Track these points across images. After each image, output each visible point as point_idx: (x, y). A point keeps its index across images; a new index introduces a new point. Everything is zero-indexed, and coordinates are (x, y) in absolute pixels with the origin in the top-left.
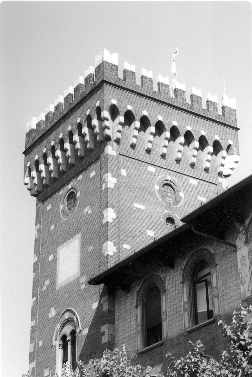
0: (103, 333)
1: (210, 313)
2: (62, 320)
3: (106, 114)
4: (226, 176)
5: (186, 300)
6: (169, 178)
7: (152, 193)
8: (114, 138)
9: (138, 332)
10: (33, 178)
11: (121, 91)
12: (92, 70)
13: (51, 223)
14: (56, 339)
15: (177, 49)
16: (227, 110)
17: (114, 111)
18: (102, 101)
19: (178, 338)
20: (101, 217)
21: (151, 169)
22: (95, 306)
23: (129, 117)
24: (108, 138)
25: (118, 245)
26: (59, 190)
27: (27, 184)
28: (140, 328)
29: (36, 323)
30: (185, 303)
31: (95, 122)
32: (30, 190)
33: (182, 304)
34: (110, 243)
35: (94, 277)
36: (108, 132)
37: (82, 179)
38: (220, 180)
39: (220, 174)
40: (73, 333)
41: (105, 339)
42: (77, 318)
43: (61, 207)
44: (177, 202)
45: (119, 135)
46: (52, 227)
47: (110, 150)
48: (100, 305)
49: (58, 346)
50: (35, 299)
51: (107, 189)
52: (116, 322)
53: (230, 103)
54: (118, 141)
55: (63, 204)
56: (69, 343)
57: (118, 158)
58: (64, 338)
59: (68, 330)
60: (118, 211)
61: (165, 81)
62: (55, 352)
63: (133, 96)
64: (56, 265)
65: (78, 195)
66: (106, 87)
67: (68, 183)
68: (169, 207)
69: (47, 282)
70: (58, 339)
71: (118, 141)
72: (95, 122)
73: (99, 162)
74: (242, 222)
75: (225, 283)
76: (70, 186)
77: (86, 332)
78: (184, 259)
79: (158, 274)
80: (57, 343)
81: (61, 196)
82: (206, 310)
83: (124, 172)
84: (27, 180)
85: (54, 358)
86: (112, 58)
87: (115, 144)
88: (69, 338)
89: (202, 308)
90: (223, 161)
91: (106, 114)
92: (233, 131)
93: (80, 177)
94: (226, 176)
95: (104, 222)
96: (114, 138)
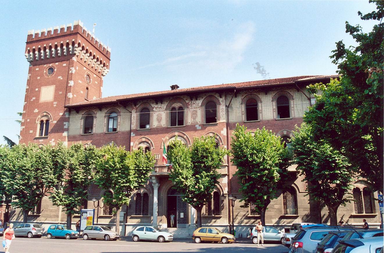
0: (65, 125)
1: (114, 130)
2: (42, 115)
3: (76, 45)
4: (104, 76)
5: (105, 123)
6: (89, 73)
7: (84, 77)
8: (77, 55)
9: (81, 128)
10: (31, 55)
11: (82, 38)
12: (72, 25)
13: (38, 76)
14: (38, 121)
15: (96, 24)
16: (108, 52)
17: (79, 45)
18: (76, 40)
19: (100, 134)
20: (68, 83)
21: (85, 68)
22: (61, 114)
23: (83, 48)
24: (75, 54)
25: (73, 95)
26: (44, 64)
27: (26, 56)
28: (82, 127)
29: (26, 112)
30: (105, 124)
31: (70, 46)
32: (27, 59)
33: (104, 124)
34: (71, 94)
35: (376, 201)
36: (75, 52)
37: (58, 65)
38: (102, 77)
39: (102, 75)
40: (47, 121)
41: (66, 127)
42: (51, 116)
43: (45, 72)
44: (90, 82)
45: (79, 54)
46: (39, 78)
47: (74, 59)
48: (64, 115)
49: (38, 123)
50: (26, 103)
51: (72, 74)
52: (70, 122)
53: (109, 50)
54: (77, 56)
55: (46, 70)
56: (45, 124)
57: (76, 63)
58: (42, 122)
59: (45, 119)
60: (74, 83)
61: (90, 33)
62: (37, 125)
63: (85, 40)
64: (40, 93)
65: (55, 70)
66: (78, 35)
67: (50, 63)
68: (88, 84)
69: (34, 98)
70: (39, 121)
71: (77, 56)
72: (70, 46)
73: (69, 61)
74: (135, 106)
75: (123, 122)
76: (51, 65)
77: (55, 122)
78: (107, 110)
79: (94, 111)
80: (38, 123)
81: (45, 67)
82: (112, 127)
83: (77, 68)
84: (27, 54)
85: (36, 127)
86: (81, 24)
87: (76, 57)
88: (45, 122)
89: (111, 126)
90: (105, 71)
91: (76, 45)
92: (109, 60)
93: (57, 64)
94: (104, 76)
95: (69, 85)
96: (77, 55)
